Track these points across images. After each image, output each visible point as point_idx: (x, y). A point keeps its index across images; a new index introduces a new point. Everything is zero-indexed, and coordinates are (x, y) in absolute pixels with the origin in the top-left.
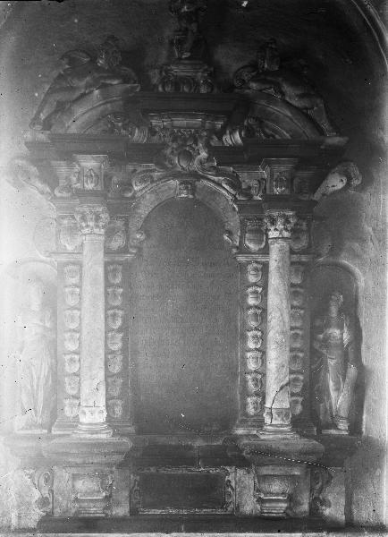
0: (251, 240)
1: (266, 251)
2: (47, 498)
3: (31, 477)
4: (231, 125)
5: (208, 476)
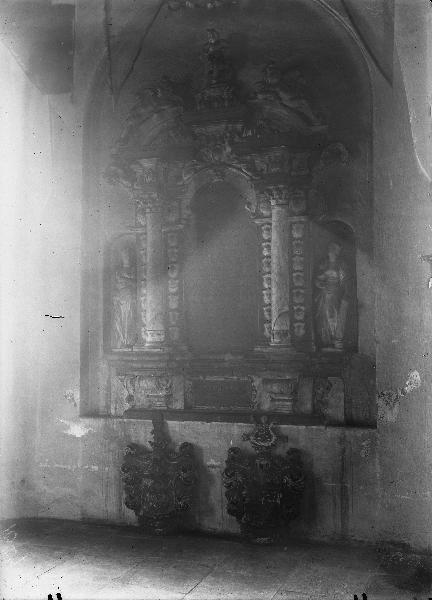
3: (122, 381)
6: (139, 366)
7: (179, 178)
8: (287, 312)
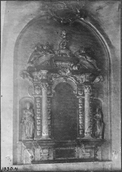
0: (80, 93)
1: (84, 95)
2: (33, 156)
4: (75, 65)
5: (71, 150)
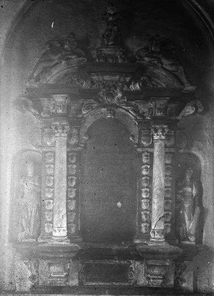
6: (52, 256)
7: (80, 111)
8: (142, 211)
